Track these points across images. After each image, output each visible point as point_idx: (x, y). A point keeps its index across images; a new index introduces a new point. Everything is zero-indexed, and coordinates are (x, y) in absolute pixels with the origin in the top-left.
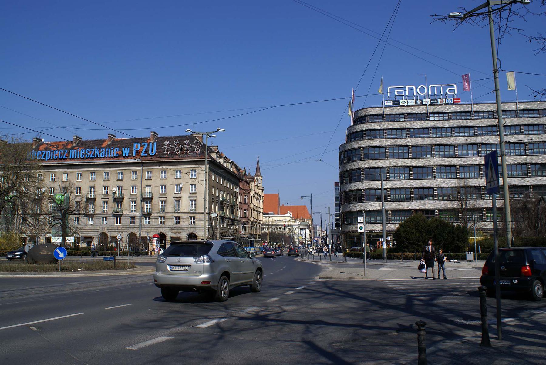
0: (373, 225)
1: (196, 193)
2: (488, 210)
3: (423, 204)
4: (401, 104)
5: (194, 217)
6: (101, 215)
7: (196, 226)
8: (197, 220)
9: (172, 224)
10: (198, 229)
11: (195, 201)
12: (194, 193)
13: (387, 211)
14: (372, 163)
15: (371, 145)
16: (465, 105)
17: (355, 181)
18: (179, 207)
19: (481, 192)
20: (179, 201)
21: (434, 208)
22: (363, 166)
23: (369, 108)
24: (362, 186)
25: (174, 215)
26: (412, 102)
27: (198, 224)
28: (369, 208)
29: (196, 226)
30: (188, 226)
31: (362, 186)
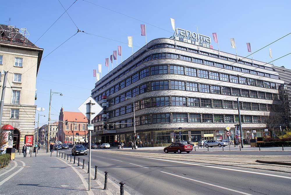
0: (179, 124)
1: (21, 84)
2: (236, 116)
3: (206, 110)
4: (184, 41)
5: (18, 110)
6: (11, 107)
7: (19, 121)
8: (22, 113)
9: (8, 118)
10: (23, 123)
11: (19, 92)
12: (18, 83)
13: (242, 116)
14: (176, 77)
15: (176, 63)
16: (216, 51)
17: (163, 89)
18: (19, 99)
19: (152, 102)
20: (19, 92)
21: (212, 113)
22: (170, 78)
23: (167, 38)
24: (170, 94)
25: (11, 107)
26: (189, 41)
27: (22, 118)
28: (175, 111)
29: (19, 121)
30: (8, 120)
31: (170, 94)
